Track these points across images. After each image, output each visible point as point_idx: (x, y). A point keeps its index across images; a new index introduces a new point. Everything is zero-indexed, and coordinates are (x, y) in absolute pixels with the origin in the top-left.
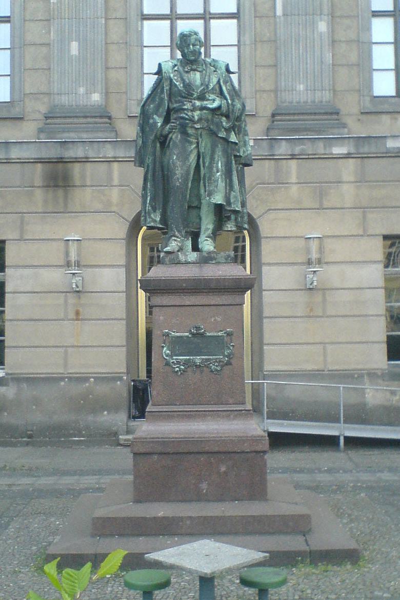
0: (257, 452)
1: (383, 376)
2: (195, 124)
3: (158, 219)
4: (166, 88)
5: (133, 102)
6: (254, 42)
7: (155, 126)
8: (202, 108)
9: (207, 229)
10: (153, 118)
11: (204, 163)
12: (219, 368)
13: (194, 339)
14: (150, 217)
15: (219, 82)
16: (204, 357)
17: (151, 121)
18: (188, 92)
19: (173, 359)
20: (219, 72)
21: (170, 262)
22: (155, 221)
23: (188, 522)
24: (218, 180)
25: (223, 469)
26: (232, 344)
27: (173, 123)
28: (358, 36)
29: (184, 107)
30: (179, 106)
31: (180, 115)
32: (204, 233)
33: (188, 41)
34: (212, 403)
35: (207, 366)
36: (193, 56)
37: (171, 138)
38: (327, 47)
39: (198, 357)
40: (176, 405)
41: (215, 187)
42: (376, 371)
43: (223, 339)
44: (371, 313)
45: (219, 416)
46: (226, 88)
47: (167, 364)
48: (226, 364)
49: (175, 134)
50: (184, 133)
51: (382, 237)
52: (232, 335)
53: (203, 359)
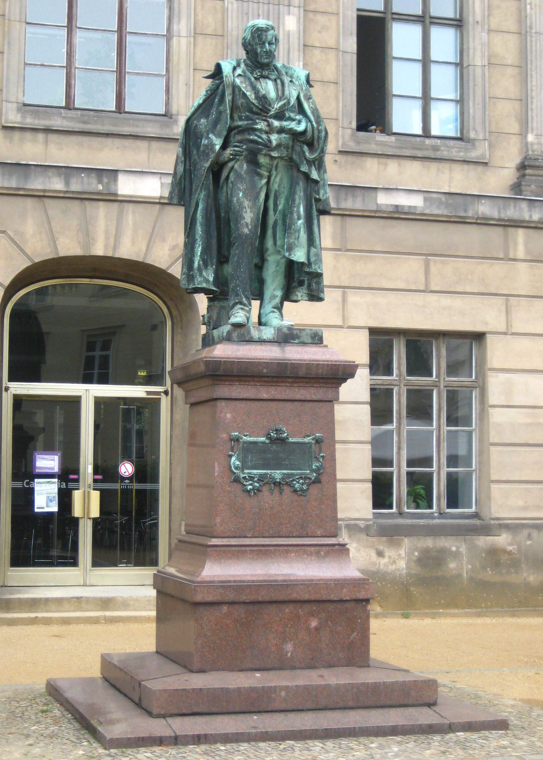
0: (357, 601)
1: (367, 528)
2: (272, 150)
3: (211, 279)
4: (228, 98)
5: (10, 105)
6: (192, 35)
7: (211, 149)
8: (281, 131)
9: (274, 297)
10: (208, 138)
11: (276, 205)
12: (305, 487)
13: (272, 447)
14: (201, 275)
15: (298, 98)
16: (285, 472)
17: (205, 142)
18: (262, 109)
19: (244, 473)
20: (297, 83)
21: (238, 338)
22: (207, 281)
23: (283, 694)
24: (300, 230)
25: (314, 623)
26: (321, 454)
27: (236, 146)
28: (338, 42)
29: (256, 126)
30: (247, 124)
31: (248, 137)
32: (270, 302)
33: (264, 37)
34: (294, 534)
35: (289, 485)
36: (267, 58)
37: (232, 168)
38: (296, 53)
39: (278, 472)
40: (247, 537)
41: (295, 239)
42: (358, 522)
43: (311, 447)
44: (351, 438)
45: (305, 552)
46: (309, 105)
47: (237, 480)
48: (314, 482)
49: (238, 163)
50: (253, 162)
51: (366, 332)
52: (321, 442)
53: (284, 474)
